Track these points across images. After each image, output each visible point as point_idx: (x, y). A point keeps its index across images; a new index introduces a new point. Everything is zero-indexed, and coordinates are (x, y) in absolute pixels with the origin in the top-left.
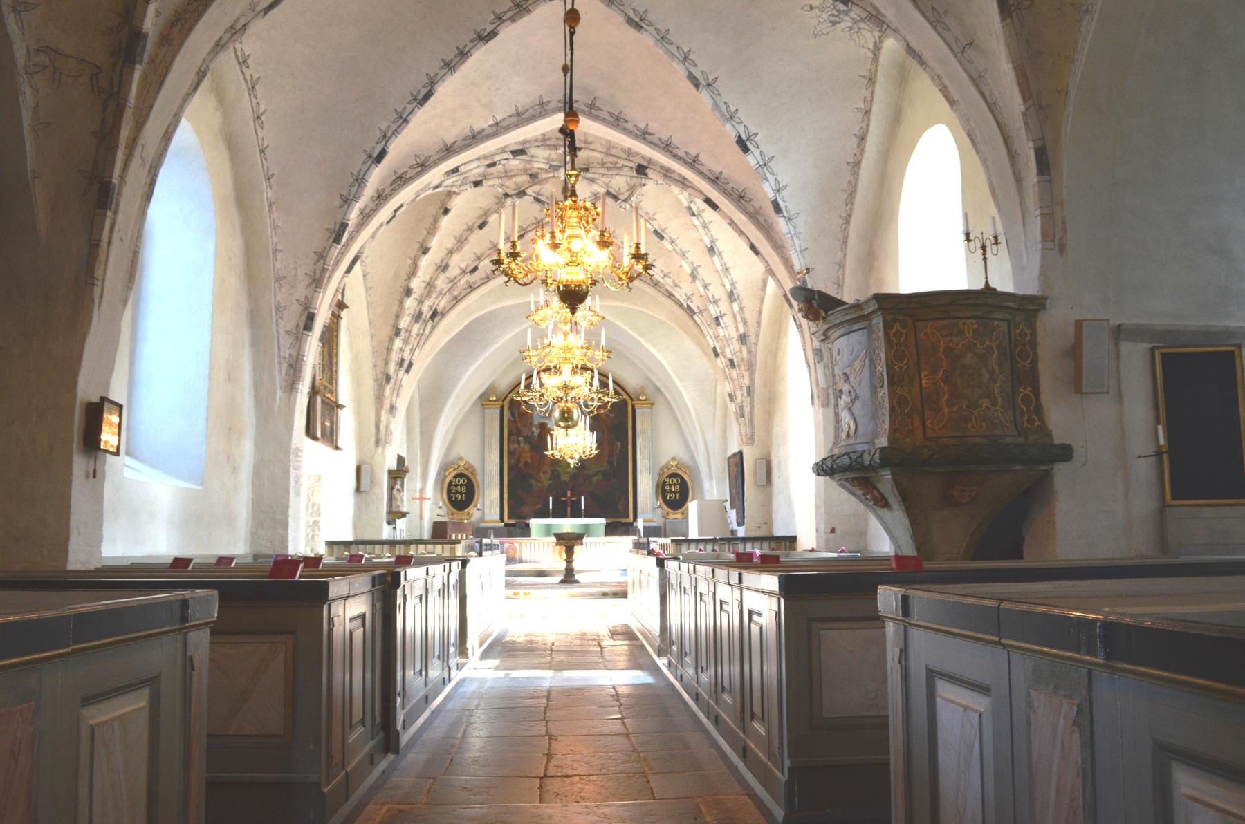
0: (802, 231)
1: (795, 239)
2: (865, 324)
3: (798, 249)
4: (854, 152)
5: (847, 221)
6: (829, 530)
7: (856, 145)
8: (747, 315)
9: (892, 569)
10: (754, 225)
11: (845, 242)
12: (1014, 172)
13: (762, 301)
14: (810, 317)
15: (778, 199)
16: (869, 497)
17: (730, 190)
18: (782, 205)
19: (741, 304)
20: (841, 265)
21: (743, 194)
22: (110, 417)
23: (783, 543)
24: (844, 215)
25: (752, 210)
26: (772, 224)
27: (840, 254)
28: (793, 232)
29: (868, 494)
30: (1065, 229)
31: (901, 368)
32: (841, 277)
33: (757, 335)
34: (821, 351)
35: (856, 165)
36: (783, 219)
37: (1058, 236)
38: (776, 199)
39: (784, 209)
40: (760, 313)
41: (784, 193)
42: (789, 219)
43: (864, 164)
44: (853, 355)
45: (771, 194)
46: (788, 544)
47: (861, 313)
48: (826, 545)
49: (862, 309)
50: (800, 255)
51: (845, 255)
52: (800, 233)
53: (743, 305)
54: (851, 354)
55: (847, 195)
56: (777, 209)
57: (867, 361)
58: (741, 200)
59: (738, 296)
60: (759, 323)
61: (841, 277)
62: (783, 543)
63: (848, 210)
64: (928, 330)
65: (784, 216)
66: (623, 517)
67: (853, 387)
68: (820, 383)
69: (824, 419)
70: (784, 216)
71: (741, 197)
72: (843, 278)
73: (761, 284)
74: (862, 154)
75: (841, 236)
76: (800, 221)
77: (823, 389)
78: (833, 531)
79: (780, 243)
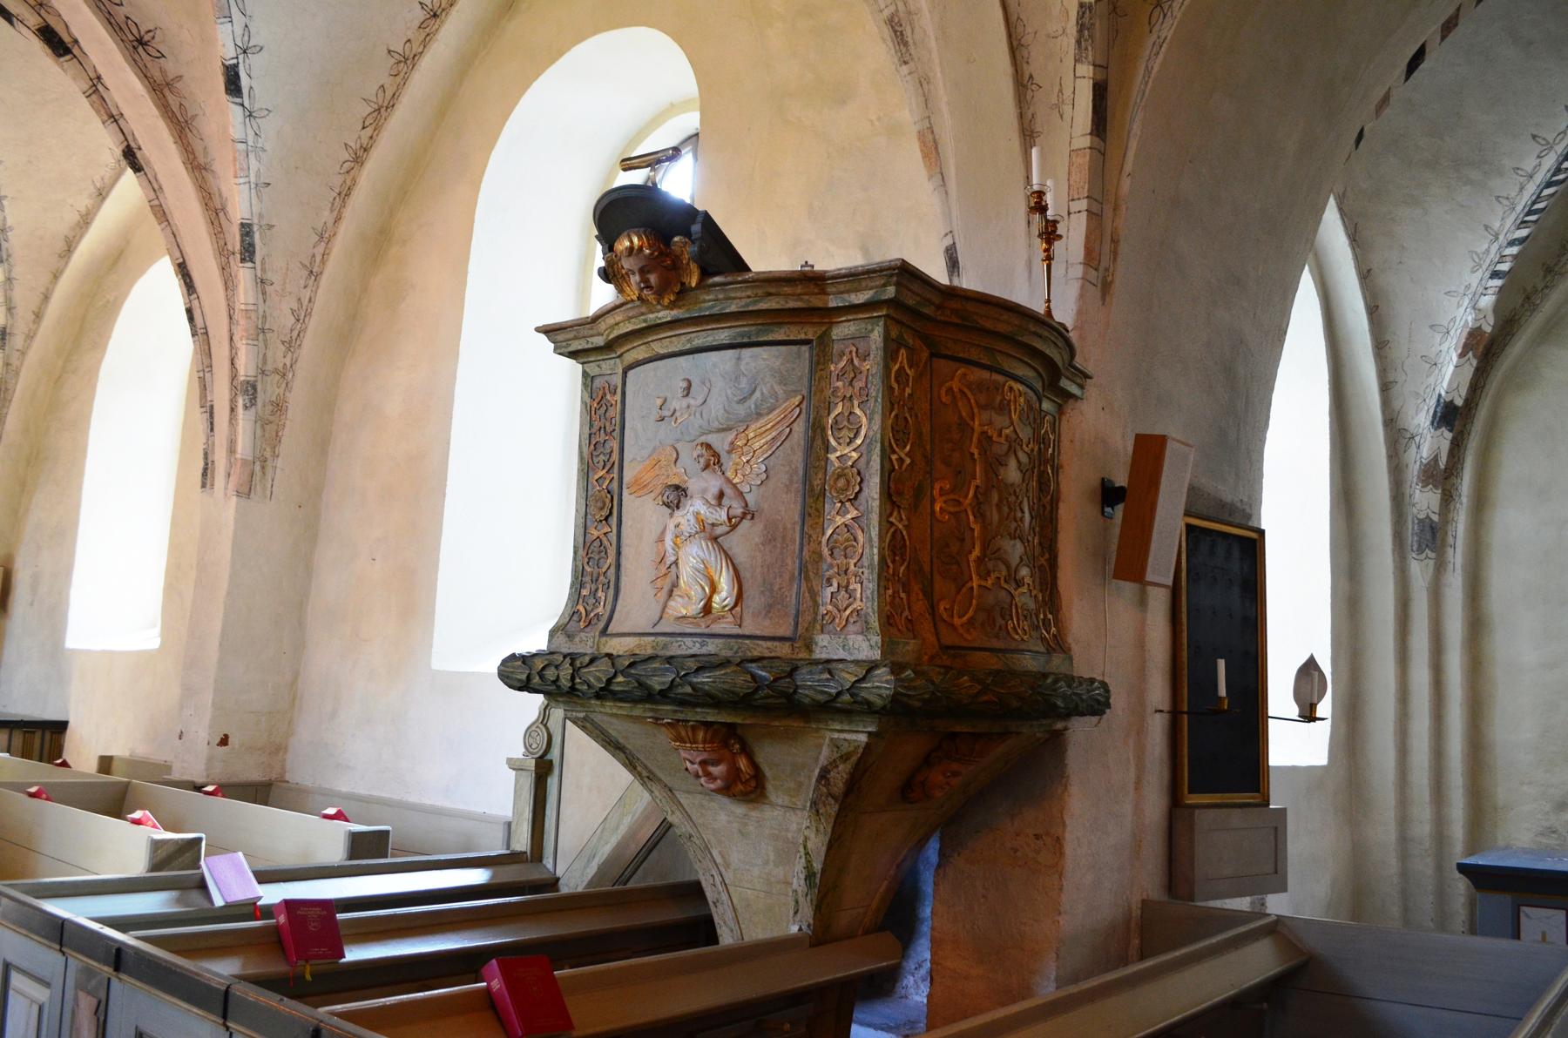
0: (267, 148)
1: (252, 156)
2: (810, 333)
3: (253, 179)
4: (410, 35)
5: (359, 156)
6: (218, 740)
7: (417, 23)
8: (18, 294)
9: (923, 1002)
10: (157, 107)
11: (345, 194)
12: (1021, 116)
13: (56, 276)
14: (653, 278)
15: (241, 66)
16: (716, 770)
17: (121, 20)
18: (245, 81)
19: (10, 271)
20: (325, 237)
21: (146, 38)
22: (858, 1015)
23: (38, 734)
24: (352, 144)
25: (157, 75)
26: (194, 117)
27: (327, 216)
28: (250, 143)
29: (716, 763)
30: (1115, 253)
31: (901, 460)
32: (318, 258)
33: (30, 337)
34: (254, 388)
35: (407, 61)
36: (240, 109)
37: (1103, 265)
38: (236, 66)
39: (245, 91)
40: (46, 298)
41: (254, 59)
42: (250, 116)
43: (426, 62)
44: (751, 403)
45: (229, 53)
46: (48, 736)
47: (816, 302)
48: (207, 770)
49: (824, 292)
50: (253, 191)
51: (338, 220)
52: (264, 150)
53: (13, 275)
54: (743, 400)
55: (371, 110)
56: (233, 84)
57: (800, 428)
58: (140, 49)
59: (9, 256)
60: (38, 316)
61: (318, 258)
62: (38, 734)
63: (365, 141)
64: (955, 385)
65: (242, 105)
66: (167, 775)
67: (729, 481)
68: (239, 448)
69: (236, 521)
70: (242, 105)
71: (141, 42)
72: (323, 262)
73: (60, 246)
74: (425, 43)
75: (337, 181)
76: (269, 125)
77: (244, 462)
78: (224, 741)
79: (201, 160)
